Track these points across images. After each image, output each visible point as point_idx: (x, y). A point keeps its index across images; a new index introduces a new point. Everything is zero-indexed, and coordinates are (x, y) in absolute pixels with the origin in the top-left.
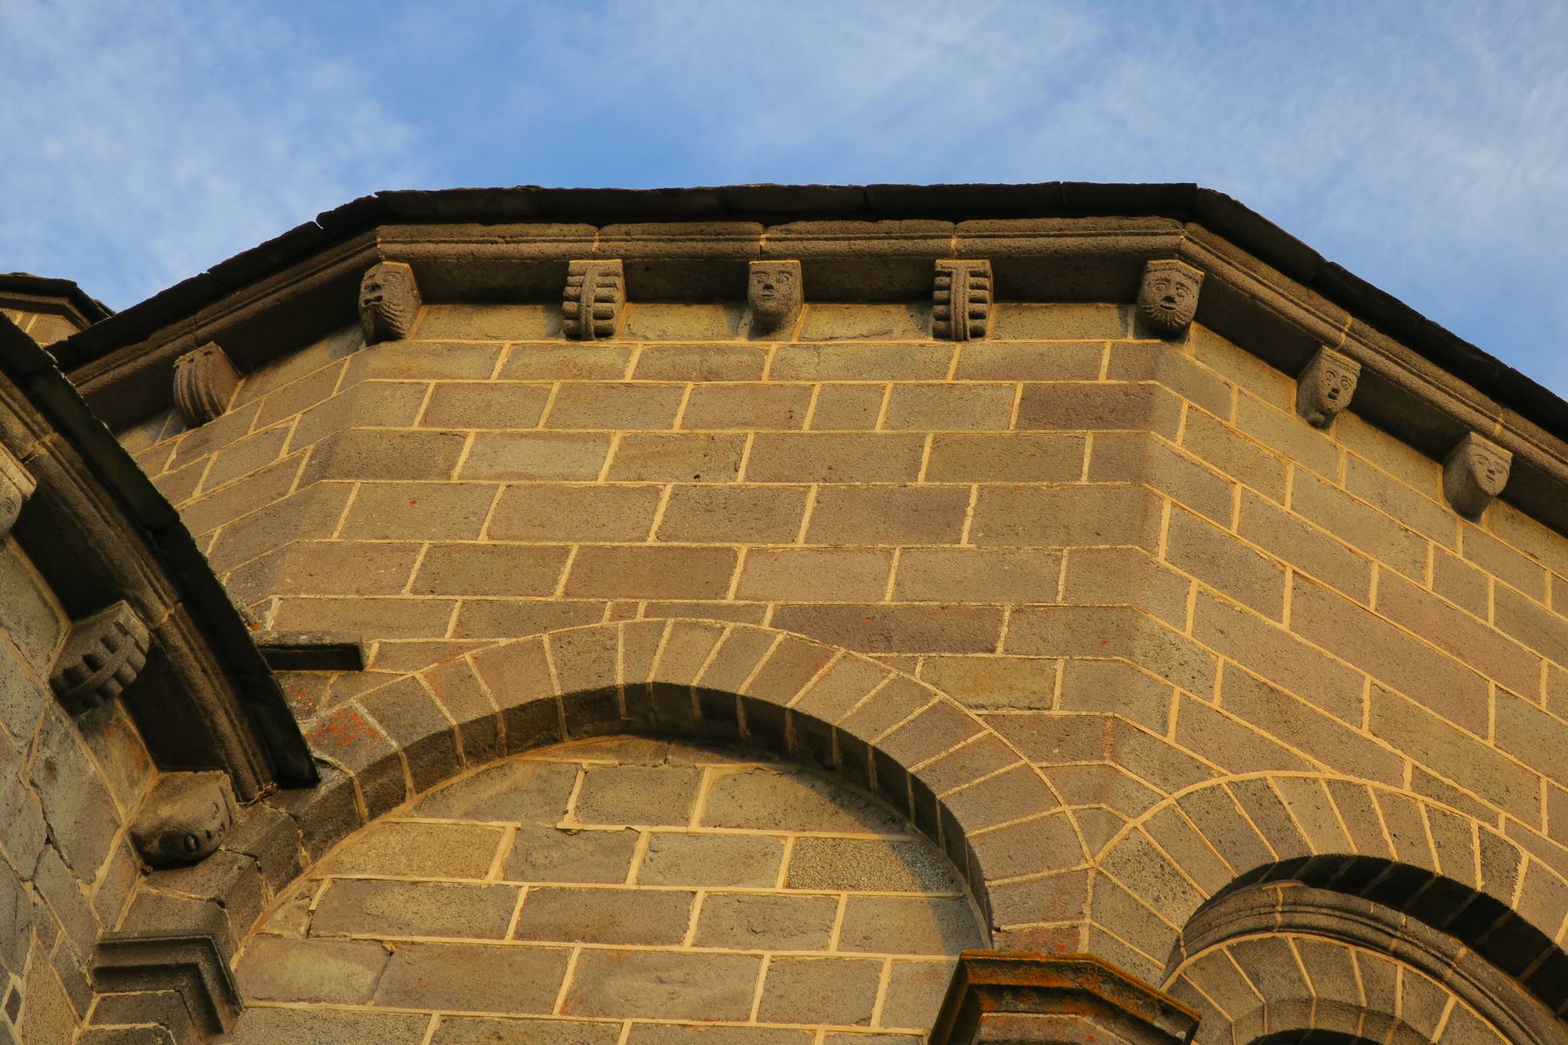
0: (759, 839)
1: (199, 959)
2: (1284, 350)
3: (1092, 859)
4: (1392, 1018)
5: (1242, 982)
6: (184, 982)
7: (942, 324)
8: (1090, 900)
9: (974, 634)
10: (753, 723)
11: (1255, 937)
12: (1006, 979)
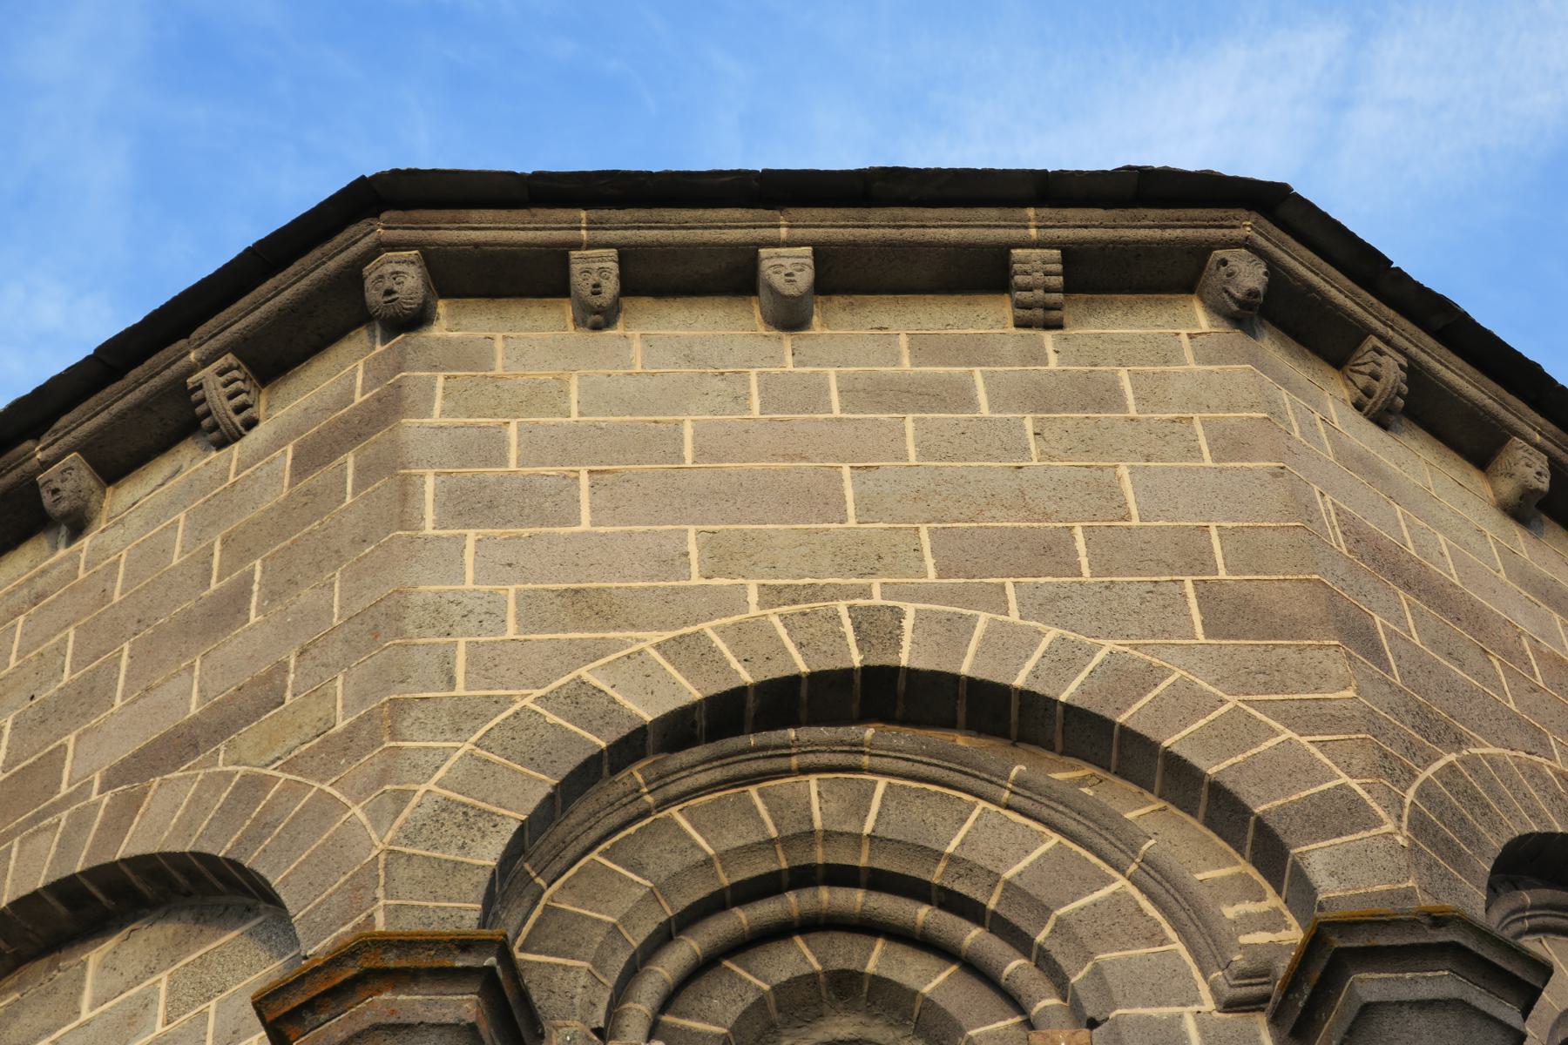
0: (138, 996)
2: (535, 278)
3: (380, 841)
4: (812, 832)
5: (622, 878)
7: (215, 435)
8: (382, 882)
9: (264, 696)
10: (109, 890)
11: (631, 830)
12: (297, 1000)
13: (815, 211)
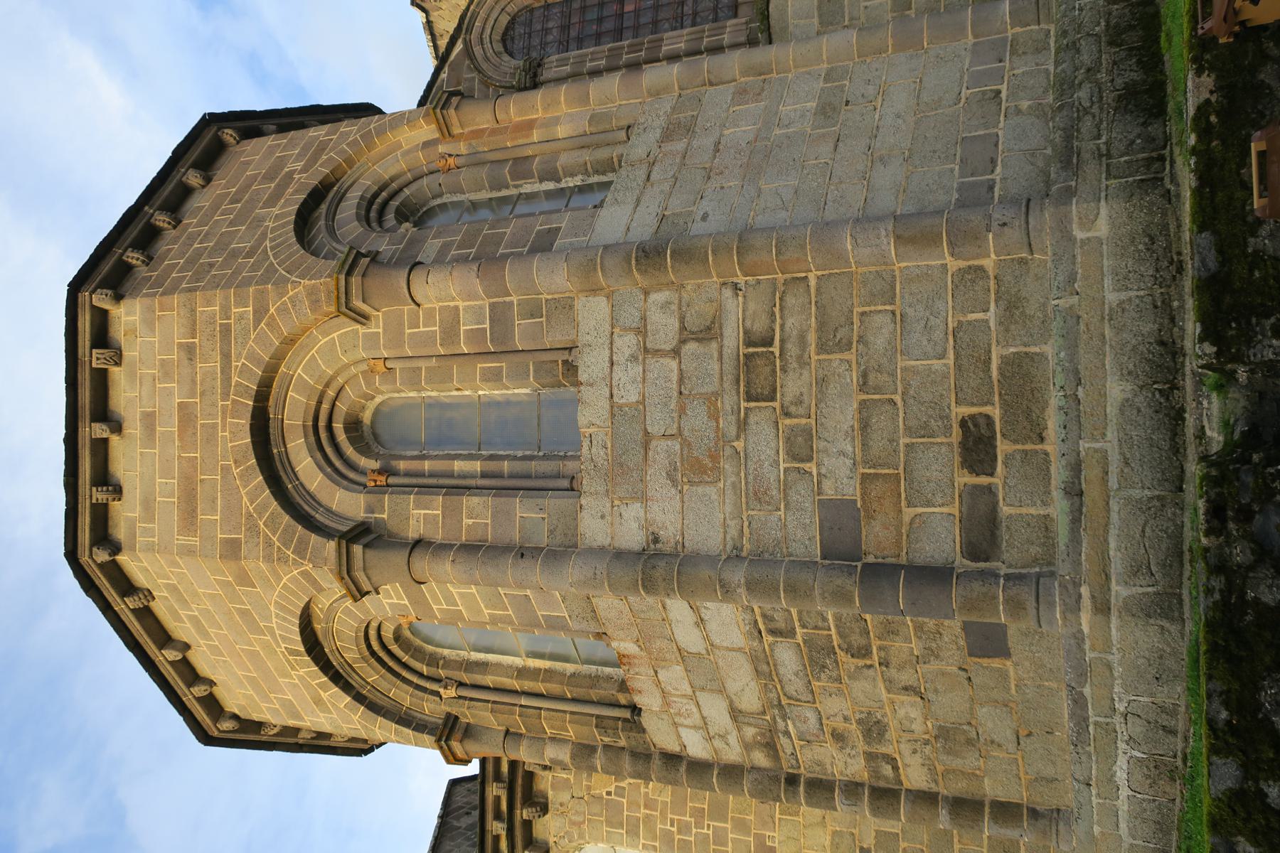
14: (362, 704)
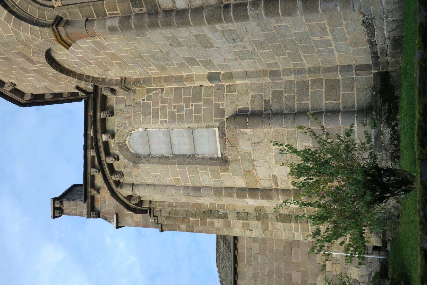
1: (123, 87)
3: (40, 40)
6: (125, 86)
13: (6, 94)
14: (14, 15)
